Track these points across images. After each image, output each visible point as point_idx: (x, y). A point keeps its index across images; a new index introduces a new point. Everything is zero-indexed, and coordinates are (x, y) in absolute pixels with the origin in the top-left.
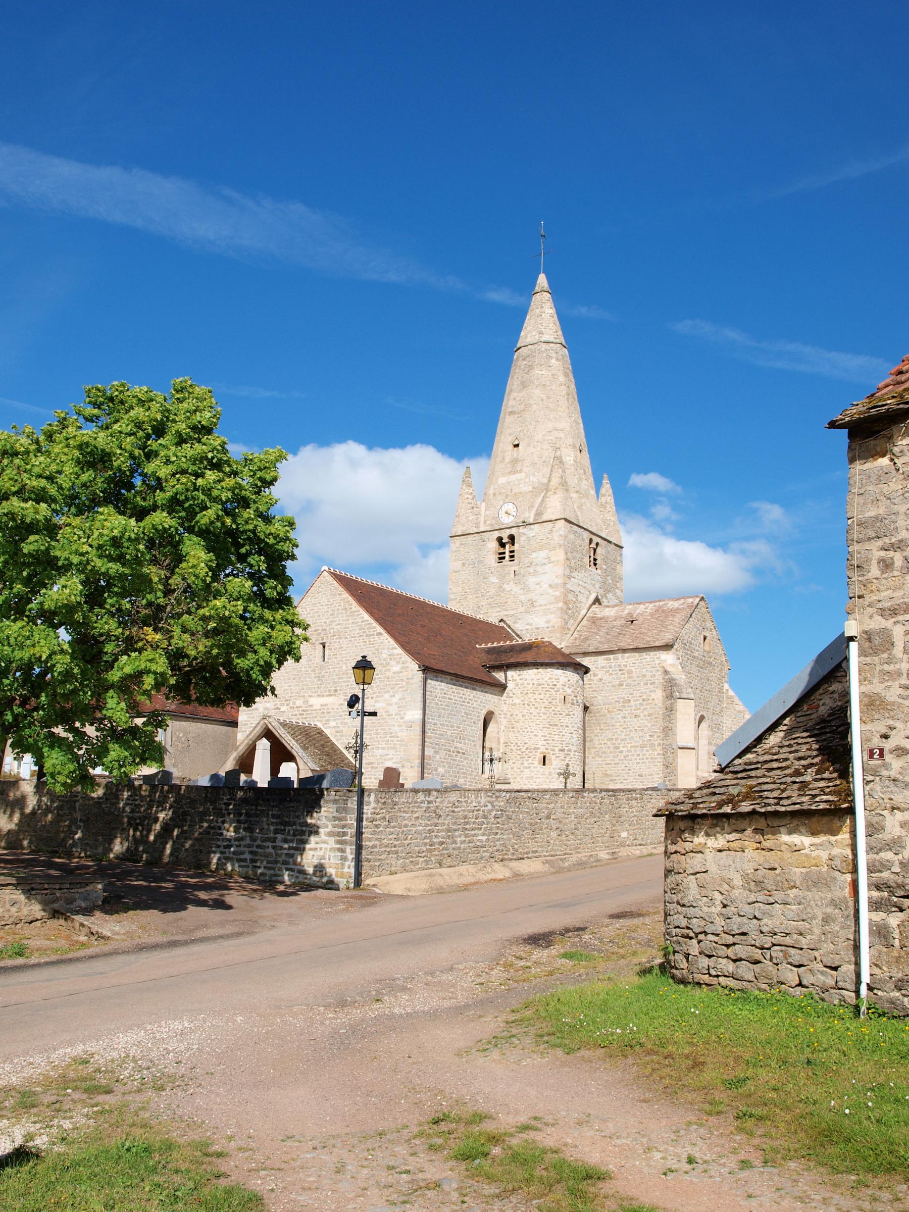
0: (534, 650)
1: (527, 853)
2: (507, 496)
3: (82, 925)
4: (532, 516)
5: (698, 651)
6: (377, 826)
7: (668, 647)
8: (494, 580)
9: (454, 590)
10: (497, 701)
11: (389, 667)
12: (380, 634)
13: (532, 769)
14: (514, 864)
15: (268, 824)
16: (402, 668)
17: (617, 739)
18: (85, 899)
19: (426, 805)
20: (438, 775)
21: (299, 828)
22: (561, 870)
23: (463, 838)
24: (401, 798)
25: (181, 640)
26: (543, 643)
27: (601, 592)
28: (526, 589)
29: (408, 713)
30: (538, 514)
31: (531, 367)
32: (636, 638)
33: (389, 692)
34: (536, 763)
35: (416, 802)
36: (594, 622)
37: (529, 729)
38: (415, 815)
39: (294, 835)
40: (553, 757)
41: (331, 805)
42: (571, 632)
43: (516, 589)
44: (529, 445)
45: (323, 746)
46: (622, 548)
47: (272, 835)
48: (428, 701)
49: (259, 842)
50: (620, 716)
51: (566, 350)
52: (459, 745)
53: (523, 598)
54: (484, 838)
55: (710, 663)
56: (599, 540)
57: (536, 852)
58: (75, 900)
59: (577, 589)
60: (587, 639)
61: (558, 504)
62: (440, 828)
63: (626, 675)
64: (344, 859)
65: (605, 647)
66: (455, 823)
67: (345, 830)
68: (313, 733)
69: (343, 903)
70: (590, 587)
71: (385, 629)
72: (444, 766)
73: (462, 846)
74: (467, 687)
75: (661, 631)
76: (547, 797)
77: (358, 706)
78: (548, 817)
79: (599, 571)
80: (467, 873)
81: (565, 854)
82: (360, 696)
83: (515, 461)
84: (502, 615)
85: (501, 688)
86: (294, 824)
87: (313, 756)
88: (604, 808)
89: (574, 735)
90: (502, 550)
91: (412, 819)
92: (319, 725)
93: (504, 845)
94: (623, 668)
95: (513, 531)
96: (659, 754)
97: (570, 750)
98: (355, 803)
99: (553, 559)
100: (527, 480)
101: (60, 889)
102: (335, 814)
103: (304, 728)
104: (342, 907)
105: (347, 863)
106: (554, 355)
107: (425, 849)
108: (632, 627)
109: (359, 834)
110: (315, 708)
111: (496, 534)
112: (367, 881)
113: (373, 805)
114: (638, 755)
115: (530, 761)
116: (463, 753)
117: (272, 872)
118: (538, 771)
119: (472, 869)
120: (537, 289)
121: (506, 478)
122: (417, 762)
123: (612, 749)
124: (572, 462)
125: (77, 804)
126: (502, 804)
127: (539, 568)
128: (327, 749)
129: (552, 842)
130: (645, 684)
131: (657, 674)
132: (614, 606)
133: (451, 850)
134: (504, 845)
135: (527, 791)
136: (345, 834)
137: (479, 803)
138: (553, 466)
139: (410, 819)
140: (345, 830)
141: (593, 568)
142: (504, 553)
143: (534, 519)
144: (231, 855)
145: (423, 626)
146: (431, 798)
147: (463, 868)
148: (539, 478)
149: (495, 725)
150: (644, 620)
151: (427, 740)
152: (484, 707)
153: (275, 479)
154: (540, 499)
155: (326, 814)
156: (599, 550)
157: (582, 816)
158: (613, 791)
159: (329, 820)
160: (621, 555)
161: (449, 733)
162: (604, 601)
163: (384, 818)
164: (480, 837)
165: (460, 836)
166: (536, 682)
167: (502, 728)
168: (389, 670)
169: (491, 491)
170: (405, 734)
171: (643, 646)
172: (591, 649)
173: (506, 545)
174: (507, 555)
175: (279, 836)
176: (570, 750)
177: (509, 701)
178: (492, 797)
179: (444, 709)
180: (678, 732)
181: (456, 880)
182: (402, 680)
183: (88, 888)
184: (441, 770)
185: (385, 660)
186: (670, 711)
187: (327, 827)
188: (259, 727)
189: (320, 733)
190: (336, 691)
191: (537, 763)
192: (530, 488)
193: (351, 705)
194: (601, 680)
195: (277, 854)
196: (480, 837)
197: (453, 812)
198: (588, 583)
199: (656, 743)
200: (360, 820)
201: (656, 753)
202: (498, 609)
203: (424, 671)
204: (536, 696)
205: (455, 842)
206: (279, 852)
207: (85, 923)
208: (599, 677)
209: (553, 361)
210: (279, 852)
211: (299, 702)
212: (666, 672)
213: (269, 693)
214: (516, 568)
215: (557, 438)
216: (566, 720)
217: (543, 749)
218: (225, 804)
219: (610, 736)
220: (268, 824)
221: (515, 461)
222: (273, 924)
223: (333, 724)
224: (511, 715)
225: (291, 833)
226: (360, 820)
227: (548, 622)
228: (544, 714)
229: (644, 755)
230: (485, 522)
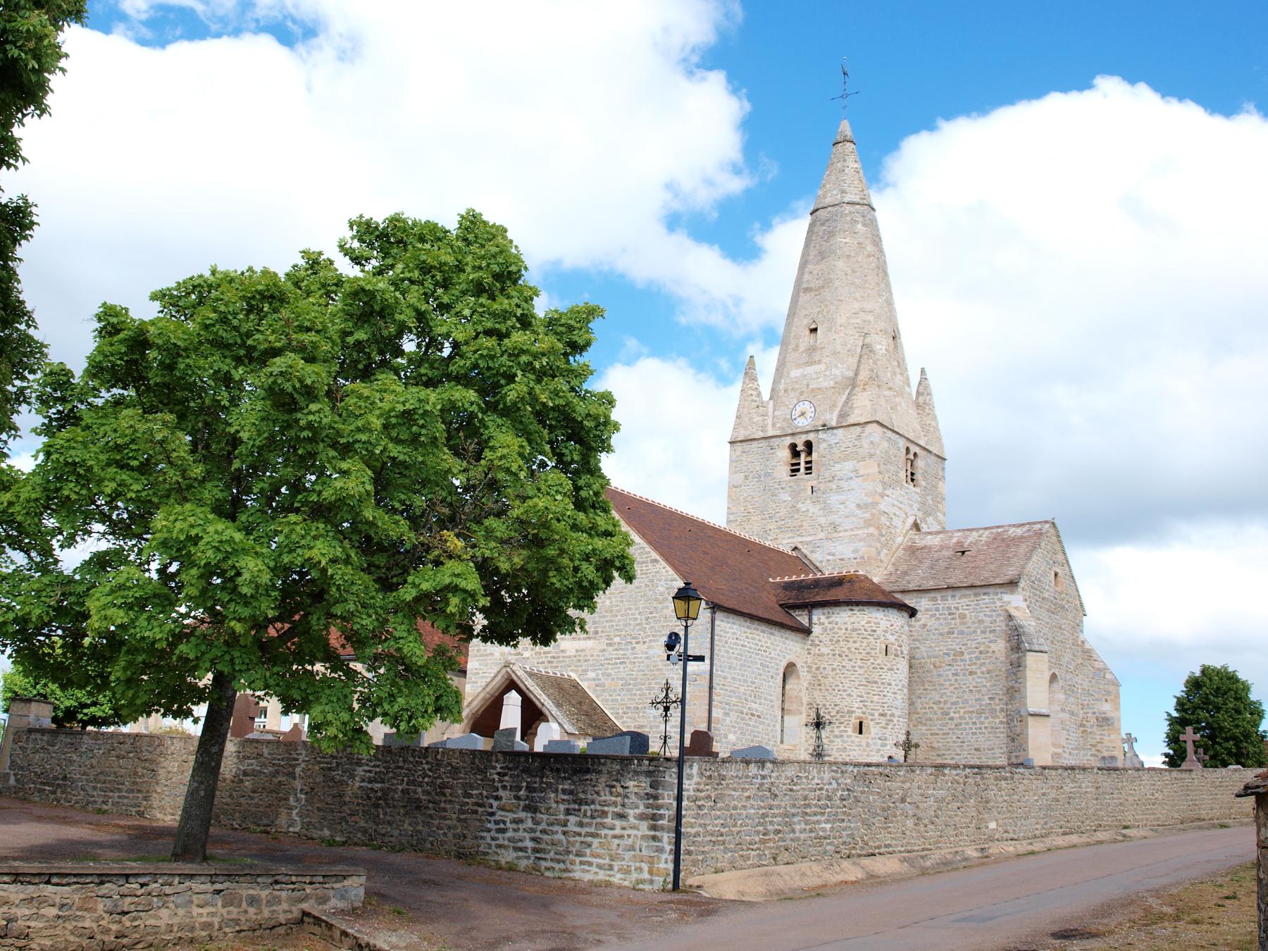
0: (847, 586)
1: (879, 847)
2: (802, 393)
3: (344, 934)
6: (699, 807)
7: (1012, 584)
12: (656, 561)
14: (866, 862)
15: (555, 803)
17: (945, 702)
18: (343, 898)
19: (759, 781)
20: (728, 743)
21: (599, 807)
22: (924, 872)
23: (803, 826)
24: (731, 771)
25: (487, 549)
26: (857, 576)
27: (920, 514)
28: (827, 509)
30: (842, 416)
31: (832, 234)
32: (970, 574)
35: (747, 777)
36: (913, 552)
37: (840, 687)
38: (746, 794)
39: (592, 817)
40: (872, 723)
41: (642, 778)
43: (814, 510)
44: (829, 330)
45: (580, 703)
47: (562, 817)
48: (716, 648)
49: (543, 826)
52: (754, 706)
53: (822, 521)
54: (828, 826)
56: (917, 450)
57: (890, 845)
58: (329, 899)
59: (891, 510)
60: (905, 573)
61: (868, 403)
62: (776, 811)
64: (660, 850)
65: (930, 584)
66: (794, 805)
67: (662, 812)
68: (566, 686)
69: (671, 909)
70: (907, 509)
71: (662, 555)
72: (735, 733)
73: (802, 836)
75: (1002, 565)
77: (679, 648)
78: (903, 800)
79: (918, 490)
80: (809, 873)
81: (924, 850)
82: (682, 634)
83: (812, 350)
84: (796, 541)
85: (807, 632)
86: (593, 802)
87: (569, 715)
88: (968, 790)
90: (794, 461)
91: (742, 797)
92: (574, 676)
93: (852, 836)
95: (811, 437)
96: (1001, 722)
97: (892, 715)
98: (675, 776)
99: (861, 473)
101: (311, 883)
102: (649, 790)
103: (556, 679)
104: (674, 916)
105: (664, 856)
106: (860, 219)
107: (757, 839)
108: (964, 559)
109: (679, 816)
110: (568, 654)
111: (789, 441)
112: (688, 880)
113: (696, 779)
114: (974, 723)
117: (562, 866)
119: (816, 868)
123: (939, 715)
125: (298, 770)
126: (849, 781)
127: (844, 484)
128: (585, 707)
129: (908, 833)
130: (982, 632)
132: (938, 533)
133: (789, 842)
134: (852, 836)
135: (878, 765)
136: (662, 817)
137: (822, 779)
138: (861, 356)
139: (739, 799)
140: (662, 812)
144: (506, 843)
145: (705, 553)
146: (765, 772)
147: (804, 866)
148: (842, 370)
150: (979, 551)
151: (714, 697)
153: (588, 344)
154: (844, 397)
155: (636, 790)
157: (943, 800)
158: (979, 767)
159: (641, 798)
160: (943, 469)
161: (742, 689)
162: (924, 528)
163: (709, 797)
164: (823, 825)
165: (799, 823)
166: (850, 627)
167: (805, 684)
169: (782, 387)
172: (911, 587)
173: (801, 455)
174: (803, 466)
175: (573, 819)
176: (892, 715)
177: (814, 650)
178: (836, 772)
181: (798, 882)
183: (346, 883)
184: (731, 737)
185: (661, 594)
186: (1017, 666)
187: (637, 807)
188: (499, 677)
189: (576, 686)
190: (596, 633)
191: (851, 730)
192: (832, 383)
193: (670, 647)
194: (925, 625)
195: (568, 842)
196: (823, 825)
197: (791, 790)
199: (998, 708)
200: (679, 799)
203: (713, 608)
205: (793, 831)
206: (571, 839)
207: (350, 931)
208: (922, 622)
209: (859, 226)
210: (571, 839)
212: (1010, 617)
213: (577, 629)
214: (814, 483)
216: (888, 676)
217: (858, 713)
218: (499, 774)
219: (937, 698)
220: (557, 802)
221: (812, 350)
222: (597, 937)
223: (591, 675)
224: (817, 669)
225: (589, 814)
226: (679, 799)
227: (856, 551)
229: (982, 723)
230: (774, 425)
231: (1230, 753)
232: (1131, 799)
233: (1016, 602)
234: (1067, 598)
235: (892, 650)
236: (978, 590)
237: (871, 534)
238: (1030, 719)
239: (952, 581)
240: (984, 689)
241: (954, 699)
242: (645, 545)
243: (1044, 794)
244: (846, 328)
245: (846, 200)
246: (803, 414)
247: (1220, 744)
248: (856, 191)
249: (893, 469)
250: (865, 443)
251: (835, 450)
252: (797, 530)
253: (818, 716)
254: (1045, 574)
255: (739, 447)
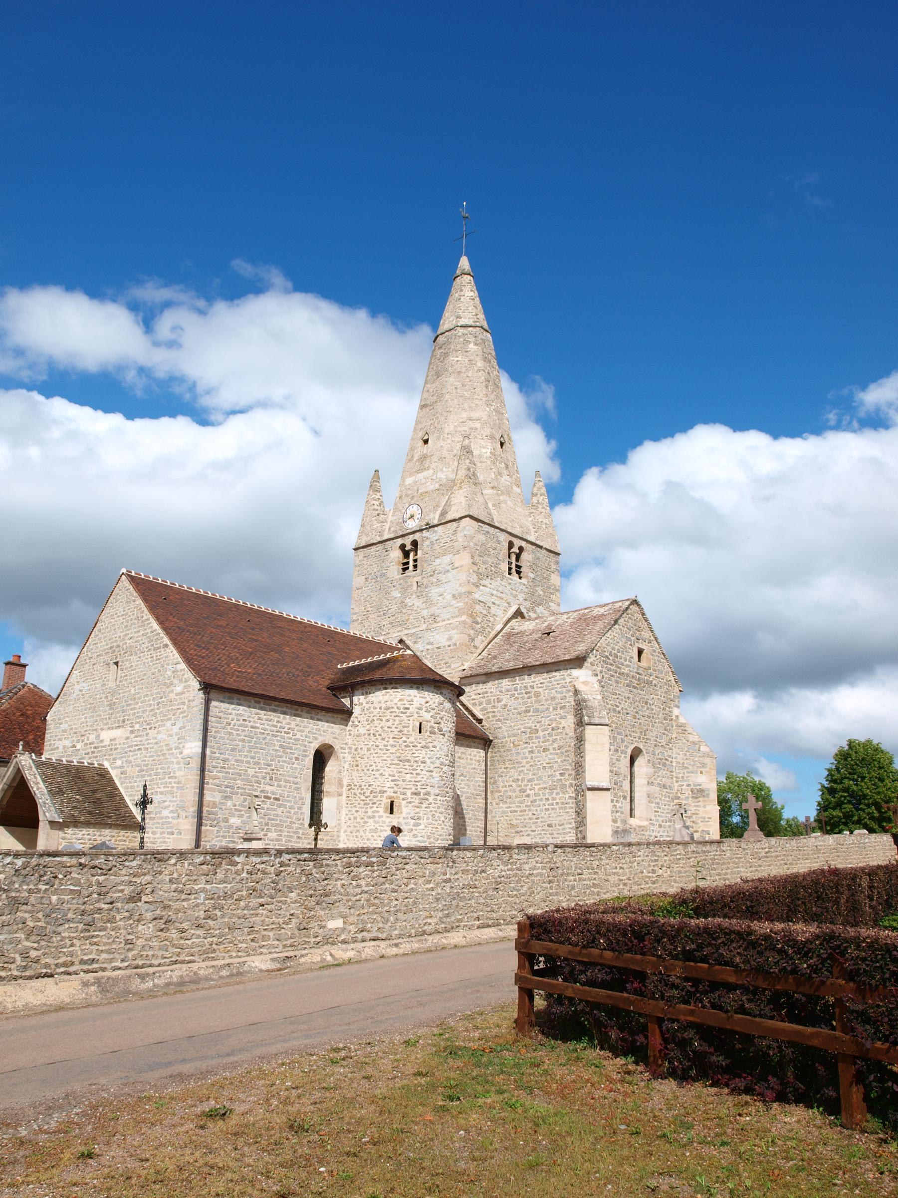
4: (437, 517)
5: (628, 666)
7: (578, 661)
8: (396, 594)
9: (356, 610)
10: (338, 732)
11: (172, 688)
12: (166, 646)
13: (377, 819)
16: (185, 687)
17: (523, 780)
28: (429, 602)
29: (187, 745)
30: (443, 513)
31: (446, 355)
33: (170, 719)
34: (381, 810)
37: (374, 767)
42: (479, 651)
43: (418, 603)
46: (559, 554)
50: (526, 750)
51: (489, 335)
53: (425, 613)
55: (650, 683)
56: (523, 544)
60: (495, 657)
61: (463, 500)
63: (533, 699)
65: (510, 665)
70: (510, 599)
72: (240, 816)
74: (284, 713)
76: (135, 863)
79: (523, 581)
83: (424, 458)
85: (347, 714)
89: (434, 774)
90: (405, 561)
92: (107, 765)
94: (530, 689)
95: (417, 536)
96: (570, 798)
97: (428, 794)
99: (456, 565)
100: (434, 477)
106: (472, 339)
111: (399, 542)
114: (547, 799)
115: (375, 809)
116: (276, 799)
118: (384, 822)
120: (458, 272)
121: (414, 477)
122: (193, 809)
123: (517, 793)
124: (488, 454)
127: (442, 577)
129: (140, 942)
131: (567, 696)
141: (515, 576)
142: (408, 563)
143: (439, 520)
149: (335, 763)
152: (316, 739)
156: (524, 556)
161: (251, 772)
167: (346, 766)
168: (172, 691)
170: (182, 773)
171: (550, 661)
174: (411, 563)
177: (354, 731)
179: (243, 740)
180: (587, 767)
182: (183, 703)
190: (124, 721)
192: (437, 486)
194: (506, 706)
198: (503, 595)
199: (567, 783)
201: (567, 796)
202: (399, 629)
204: (383, 724)
208: (503, 702)
209: (471, 345)
211: (92, 738)
212: (576, 692)
214: (418, 579)
215: (472, 428)
216: (422, 754)
217: (390, 793)
221: (424, 458)
223: (119, 763)
224: (356, 750)
227: (450, 639)
228: (392, 746)
229: (554, 799)
231: (872, 818)
232: (613, 879)
233: (584, 678)
234: (656, 674)
235: (426, 727)
236: (551, 667)
237: (464, 622)
238: (588, 793)
239: (531, 661)
240: (556, 765)
241: (531, 777)
242: (160, 631)
243: (448, 881)
244: (453, 436)
245: (461, 323)
246: (412, 516)
247: (863, 810)
248: (470, 315)
249: (490, 560)
250: (460, 536)
251: (436, 547)
252: (404, 624)
253: (145, 795)
254: (624, 649)
255: (361, 553)
